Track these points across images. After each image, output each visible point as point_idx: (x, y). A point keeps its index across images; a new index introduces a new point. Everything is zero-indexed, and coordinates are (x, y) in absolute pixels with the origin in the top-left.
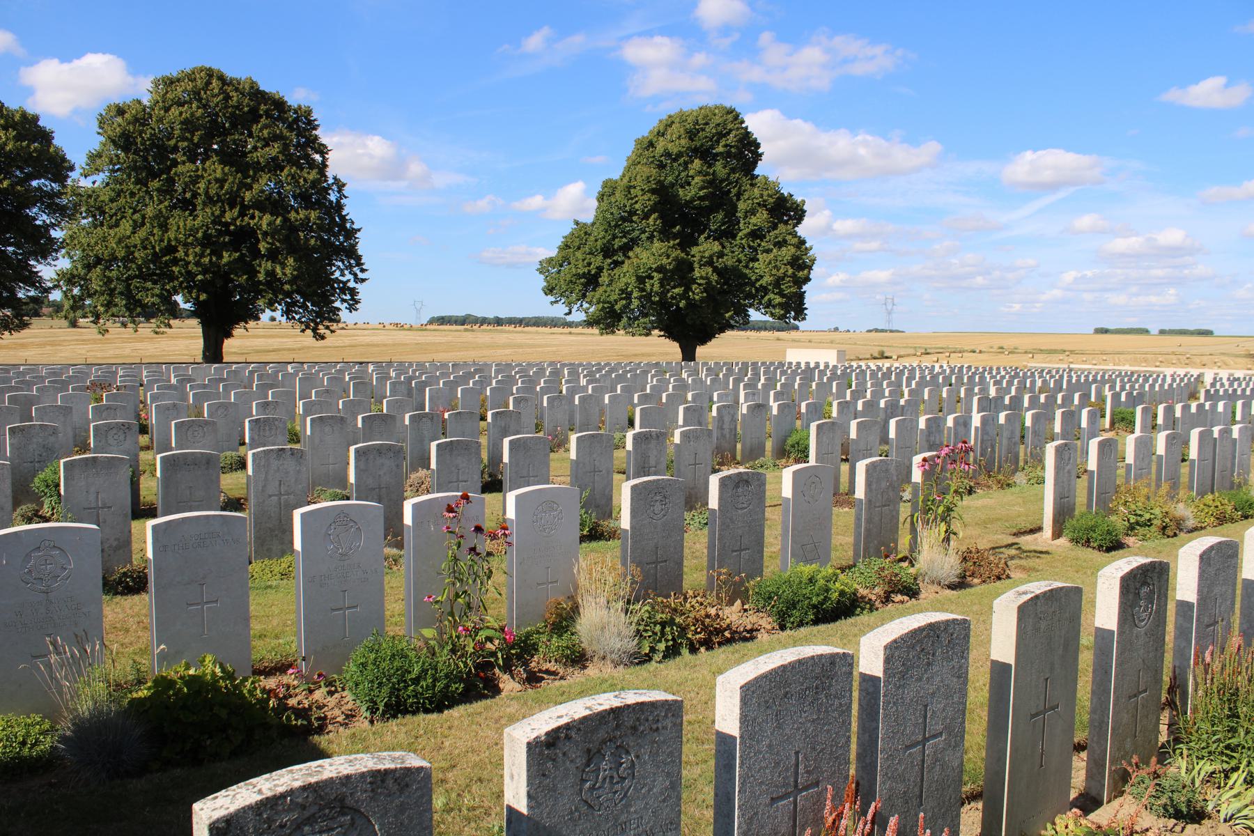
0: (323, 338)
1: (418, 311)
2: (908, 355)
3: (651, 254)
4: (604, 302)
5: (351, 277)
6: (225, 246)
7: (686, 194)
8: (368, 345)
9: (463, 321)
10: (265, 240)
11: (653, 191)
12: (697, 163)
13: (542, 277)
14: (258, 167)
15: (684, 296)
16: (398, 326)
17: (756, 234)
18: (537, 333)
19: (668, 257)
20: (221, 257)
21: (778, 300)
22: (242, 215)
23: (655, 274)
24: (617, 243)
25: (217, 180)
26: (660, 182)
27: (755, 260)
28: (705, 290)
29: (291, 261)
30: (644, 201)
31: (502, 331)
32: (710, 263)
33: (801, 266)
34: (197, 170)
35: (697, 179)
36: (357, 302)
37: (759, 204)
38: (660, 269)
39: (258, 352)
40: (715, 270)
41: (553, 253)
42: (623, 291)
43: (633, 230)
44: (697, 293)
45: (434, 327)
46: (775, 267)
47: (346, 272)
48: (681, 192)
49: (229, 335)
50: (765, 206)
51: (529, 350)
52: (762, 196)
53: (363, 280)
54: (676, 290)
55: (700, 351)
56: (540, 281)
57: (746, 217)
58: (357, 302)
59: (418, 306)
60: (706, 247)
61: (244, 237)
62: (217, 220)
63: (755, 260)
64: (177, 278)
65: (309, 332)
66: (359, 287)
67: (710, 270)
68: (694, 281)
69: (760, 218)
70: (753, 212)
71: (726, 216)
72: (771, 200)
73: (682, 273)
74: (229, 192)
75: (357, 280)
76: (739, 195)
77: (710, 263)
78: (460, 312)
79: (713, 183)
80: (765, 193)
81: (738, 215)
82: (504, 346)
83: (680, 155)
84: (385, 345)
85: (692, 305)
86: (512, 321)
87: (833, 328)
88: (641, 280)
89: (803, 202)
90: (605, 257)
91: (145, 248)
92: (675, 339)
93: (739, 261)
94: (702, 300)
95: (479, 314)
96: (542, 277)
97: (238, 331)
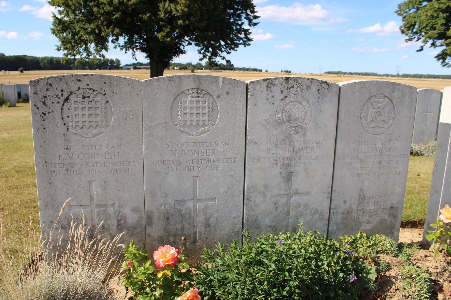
1: (320, 69)
5: (246, 22)
9: (338, 73)
16: (387, 75)
18: (431, 81)
36: (250, 40)
45: (326, 75)
64: (99, 19)
66: (252, 29)
78: (336, 70)
92: (8, 57)
96: (401, 18)
97: (165, 71)
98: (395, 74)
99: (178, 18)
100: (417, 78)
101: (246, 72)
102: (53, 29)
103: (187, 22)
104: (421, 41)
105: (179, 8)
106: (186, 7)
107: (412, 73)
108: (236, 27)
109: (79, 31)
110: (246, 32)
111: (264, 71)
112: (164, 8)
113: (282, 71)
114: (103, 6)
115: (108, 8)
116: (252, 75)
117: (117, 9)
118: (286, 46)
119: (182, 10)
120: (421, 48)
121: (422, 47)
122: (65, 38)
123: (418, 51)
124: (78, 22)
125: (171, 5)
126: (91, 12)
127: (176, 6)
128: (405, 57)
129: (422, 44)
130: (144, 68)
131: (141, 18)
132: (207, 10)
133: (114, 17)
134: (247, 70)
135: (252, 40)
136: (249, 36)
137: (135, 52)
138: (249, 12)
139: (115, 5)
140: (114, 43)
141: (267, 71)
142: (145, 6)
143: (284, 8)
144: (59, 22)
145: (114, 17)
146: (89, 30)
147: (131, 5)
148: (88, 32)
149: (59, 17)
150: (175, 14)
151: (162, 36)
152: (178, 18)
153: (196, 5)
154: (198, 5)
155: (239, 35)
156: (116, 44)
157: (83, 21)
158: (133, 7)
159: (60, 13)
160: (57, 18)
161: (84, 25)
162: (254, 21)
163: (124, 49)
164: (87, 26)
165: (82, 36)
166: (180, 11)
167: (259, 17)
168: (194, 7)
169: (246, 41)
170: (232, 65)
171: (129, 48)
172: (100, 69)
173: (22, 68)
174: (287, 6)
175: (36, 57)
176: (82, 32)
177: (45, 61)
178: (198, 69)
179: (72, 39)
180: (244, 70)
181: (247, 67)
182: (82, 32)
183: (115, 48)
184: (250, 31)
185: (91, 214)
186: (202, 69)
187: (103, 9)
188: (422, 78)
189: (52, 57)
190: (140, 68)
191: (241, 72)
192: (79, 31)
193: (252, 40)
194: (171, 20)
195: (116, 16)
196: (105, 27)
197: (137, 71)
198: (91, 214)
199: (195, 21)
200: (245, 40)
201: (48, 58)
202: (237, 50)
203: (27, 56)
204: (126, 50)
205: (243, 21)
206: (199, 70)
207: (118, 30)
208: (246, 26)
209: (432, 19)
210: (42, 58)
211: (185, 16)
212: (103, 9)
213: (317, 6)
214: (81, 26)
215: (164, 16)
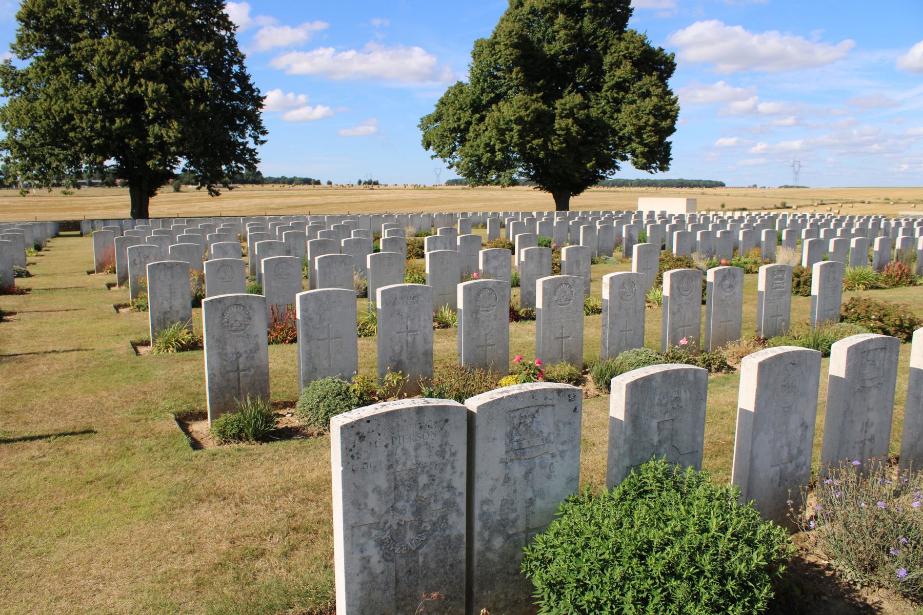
1: (438, 176)
2: (807, 206)
3: (513, 107)
4: (472, 156)
6: (119, 113)
7: (549, 49)
8: (376, 201)
10: (151, 106)
11: (515, 46)
12: (561, 18)
14: (157, 41)
15: (544, 147)
17: (621, 86)
19: (527, 109)
20: (113, 122)
21: (640, 149)
22: (132, 83)
23: (514, 126)
24: (485, 99)
25: (109, 53)
26: (522, 37)
27: (619, 111)
28: (565, 141)
29: (175, 124)
30: (506, 54)
32: (571, 114)
33: (665, 116)
34: (93, 45)
35: (562, 33)
37: (624, 56)
38: (519, 121)
39: (289, 207)
40: (576, 121)
42: (487, 145)
43: (501, 86)
44: (556, 145)
46: (637, 116)
48: (546, 47)
49: (153, 194)
50: (631, 58)
51: (497, 203)
52: (627, 49)
53: (263, 142)
54: (535, 142)
55: (574, 201)
57: (611, 70)
59: (438, 172)
60: (571, 99)
61: (135, 104)
62: (109, 90)
63: (619, 111)
65: (204, 189)
66: (259, 148)
67: (570, 121)
68: (554, 132)
69: (624, 71)
70: (617, 64)
71: (591, 69)
72: (637, 52)
73: (540, 124)
75: (257, 141)
76: (605, 49)
77: (571, 114)
79: (578, 38)
80: (631, 46)
81: (604, 68)
83: (545, 11)
85: (550, 154)
87: (752, 185)
88: (502, 132)
89: (673, 55)
90: (474, 112)
91: (48, 117)
92: (549, 189)
93: (604, 112)
94: (561, 150)
99: (172, 145)
101: (287, 186)
105: (171, 134)
106: (179, 133)
110: (252, 152)
111: (324, 183)
113: (360, 182)
115: (88, 133)
116: (296, 193)
117: (99, 135)
118: (362, 129)
134: (291, 182)
141: (330, 183)
152: (172, 145)
154: (192, 128)
162: (262, 138)
164: (57, 151)
170: (259, 173)
180: (284, 183)
181: (289, 176)
185: (20, 440)
191: (277, 186)
198: (20, 440)
208: (251, 145)
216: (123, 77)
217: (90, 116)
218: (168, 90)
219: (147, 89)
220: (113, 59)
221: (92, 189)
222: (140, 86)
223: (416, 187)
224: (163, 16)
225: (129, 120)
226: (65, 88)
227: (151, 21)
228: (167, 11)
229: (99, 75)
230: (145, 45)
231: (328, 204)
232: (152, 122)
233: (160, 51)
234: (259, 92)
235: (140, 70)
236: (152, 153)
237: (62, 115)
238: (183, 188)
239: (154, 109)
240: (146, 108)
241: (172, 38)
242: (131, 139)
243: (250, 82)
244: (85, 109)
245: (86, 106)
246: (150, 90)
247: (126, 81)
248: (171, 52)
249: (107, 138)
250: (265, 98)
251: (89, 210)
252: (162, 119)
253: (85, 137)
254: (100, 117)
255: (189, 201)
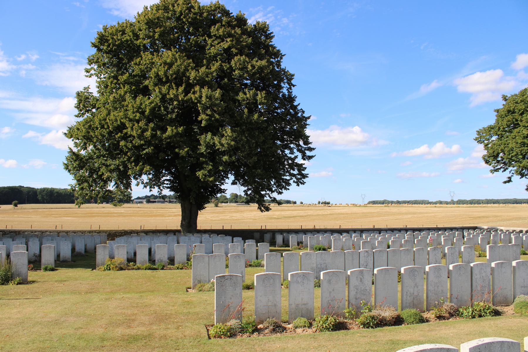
0: (268, 209)
1: (363, 199)
5: (300, 155)
6: (172, 122)
8: (339, 214)
9: (383, 202)
10: (204, 113)
13: (482, 146)
20: (164, 130)
22: (186, 92)
25: (165, 63)
31: (402, 207)
36: (305, 176)
41: (491, 120)
47: (295, 150)
49: (202, 208)
51: (420, 215)
53: (310, 158)
56: (480, 151)
58: (305, 176)
61: (188, 113)
62: (163, 99)
64: (126, 154)
66: (306, 163)
74: (177, 73)
78: (382, 199)
82: (407, 214)
84: (347, 214)
86: (408, 202)
91: (103, 127)
95: (390, 199)
96: (482, 146)
98: (449, 200)
99: (224, 153)
100: (475, 204)
102: (66, 164)
103: (233, 158)
104: (507, 171)
105: (224, 141)
107: (468, 198)
108: (288, 162)
109: (99, 168)
110: (300, 167)
111: (298, 203)
112: (205, 142)
113: (319, 203)
114: (131, 139)
115: (137, 142)
117: (148, 143)
118: (324, 173)
119: (228, 144)
120: (508, 179)
121: (510, 178)
122: (81, 176)
123: (505, 182)
124: (98, 157)
125: (215, 138)
126: (116, 146)
127: (220, 139)
128: (458, 180)
129: (510, 175)
130: (158, 202)
131: (178, 154)
132: (256, 143)
133: (145, 152)
135: (307, 177)
136: (303, 172)
137: (161, 190)
138: (301, 143)
139: (147, 138)
140: (137, 179)
141: (302, 203)
142: (182, 140)
143: (320, 131)
144: (75, 156)
145: (145, 152)
146: (112, 167)
147: (166, 138)
148: (111, 169)
149: (75, 150)
150: (219, 149)
151: (204, 175)
152: (224, 153)
153: (244, 138)
154: (246, 137)
155: (292, 171)
156: (139, 180)
157: (104, 156)
158: (169, 140)
159: (76, 145)
160: (74, 153)
161: (106, 160)
162: (308, 153)
163: (148, 187)
164: (109, 162)
165: (103, 174)
166: (226, 145)
167: (314, 149)
168: (242, 140)
169: (301, 179)
171: (154, 185)
172: (107, 203)
173: (16, 202)
174: (323, 129)
175: (33, 188)
176: (103, 170)
177: (44, 193)
178: (222, 202)
179: (89, 177)
182: (103, 170)
183: (138, 185)
184: (304, 166)
186: (227, 202)
187: (131, 142)
188: (480, 204)
189: (52, 188)
190: (155, 202)
192: (99, 168)
193: (307, 177)
194: (214, 154)
195: (147, 150)
196: (133, 164)
197: (151, 205)
199: (242, 156)
200: (299, 177)
201: (48, 189)
202: (289, 189)
203: (23, 187)
204: (151, 187)
205: (295, 155)
206: (223, 204)
207: (148, 167)
209: (524, 146)
210: (41, 189)
211: (232, 151)
212: (131, 142)
213: (356, 129)
214: (103, 162)
215: (205, 151)
216: (178, 85)
217: (142, 124)
218: (223, 98)
219: (201, 97)
220: (169, 68)
221: (171, 204)
222: (194, 93)
223: (354, 205)
224: (220, 37)
225: (180, 129)
226: (123, 98)
227: (209, 42)
228: (223, 32)
229: (156, 85)
230: (202, 62)
231: (310, 215)
232: (204, 130)
233: (215, 66)
234: (303, 112)
235: (195, 79)
236: (203, 163)
237: (115, 124)
238: (220, 205)
239: (207, 115)
240: (198, 114)
241: (228, 55)
242: (180, 148)
243: (295, 104)
244: (137, 118)
245: (138, 115)
246: (204, 95)
247: (181, 89)
248: (226, 66)
249: (156, 147)
250: (309, 118)
251: (165, 217)
252: (214, 128)
253: (134, 146)
254: (152, 125)
255: (223, 212)
